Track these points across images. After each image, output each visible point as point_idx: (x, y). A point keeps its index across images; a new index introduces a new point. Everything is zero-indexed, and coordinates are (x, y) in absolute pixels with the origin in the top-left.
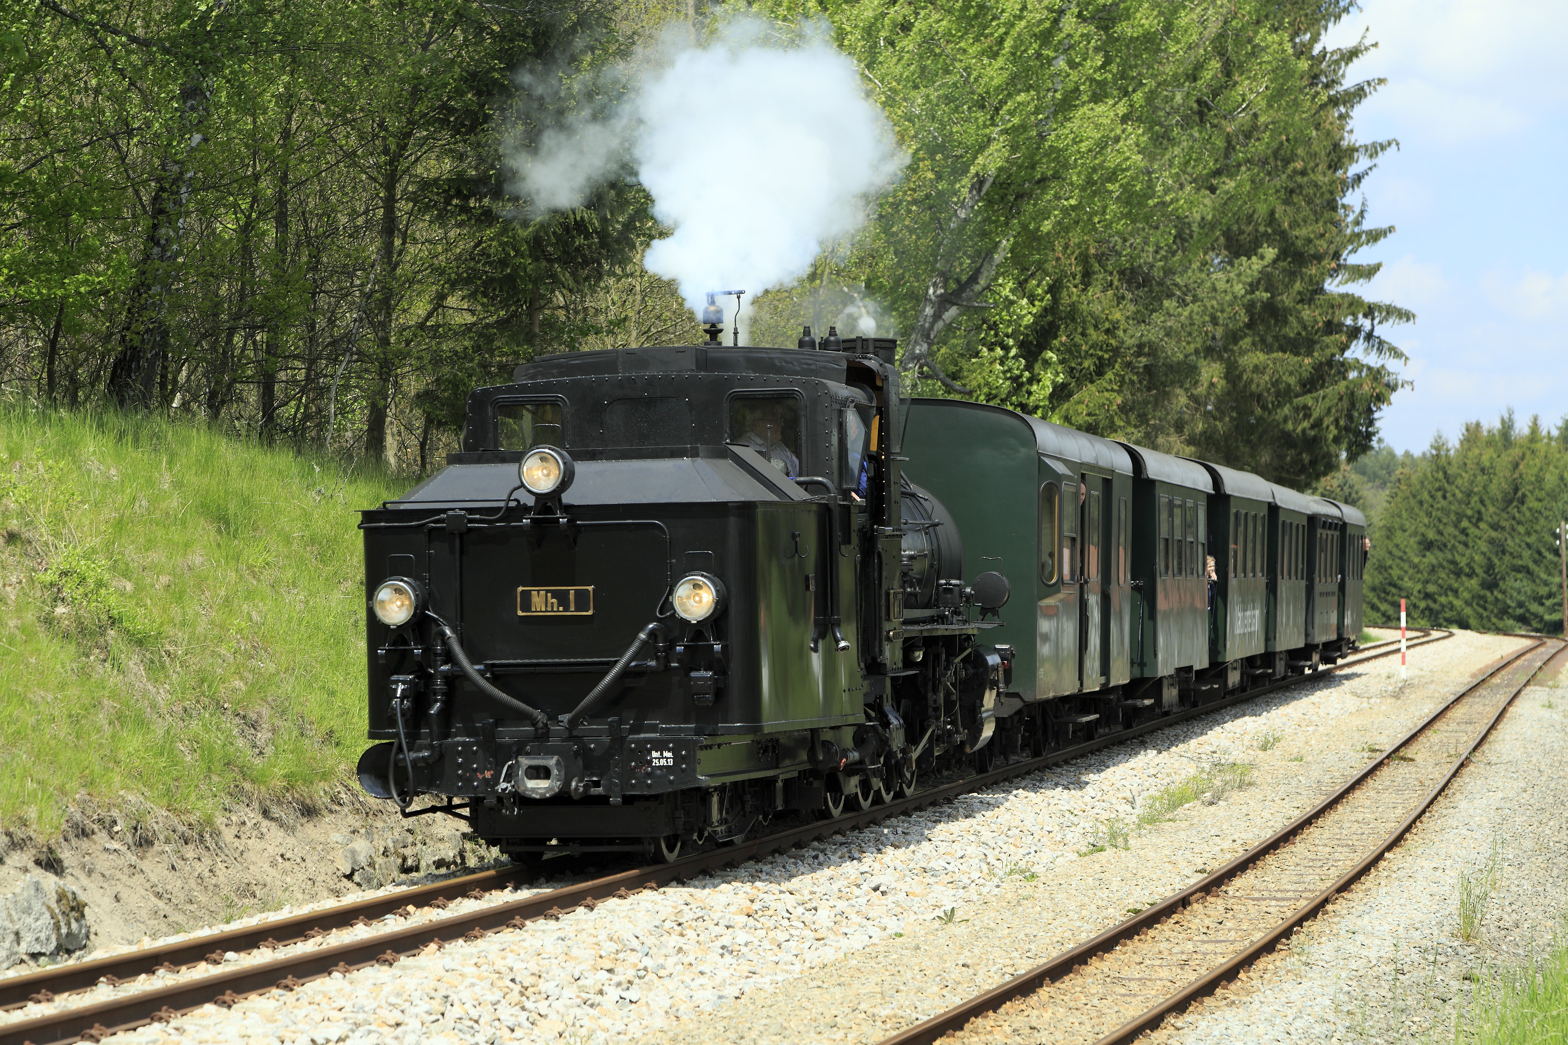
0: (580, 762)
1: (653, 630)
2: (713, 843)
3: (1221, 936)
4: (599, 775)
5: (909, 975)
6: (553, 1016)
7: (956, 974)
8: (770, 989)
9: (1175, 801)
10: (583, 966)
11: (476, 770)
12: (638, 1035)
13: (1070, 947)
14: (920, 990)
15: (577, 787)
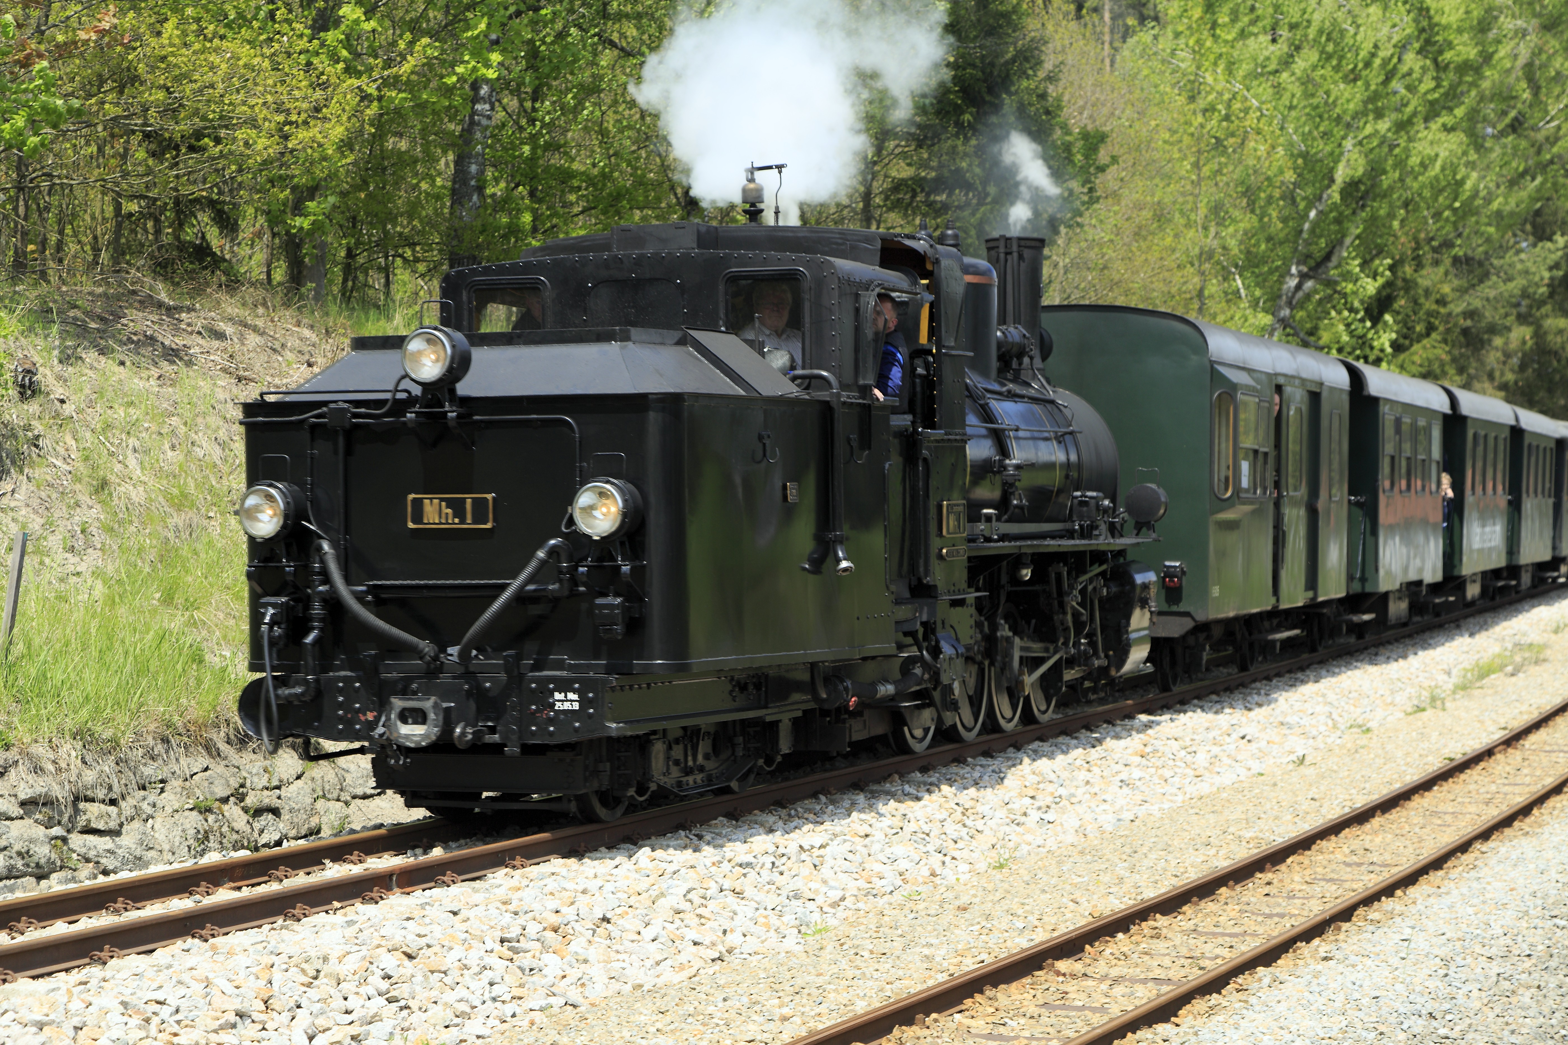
0: (472, 705)
1: (554, 546)
2: (662, 796)
3: (1518, 780)
4: (496, 719)
5: (1268, 806)
6: (987, 831)
7: (1306, 806)
8: (1158, 815)
9: (1484, 672)
10: (1012, 794)
11: (358, 711)
12: (1054, 848)
13: (1397, 786)
14: (1277, 818)
15: (463, 734)
